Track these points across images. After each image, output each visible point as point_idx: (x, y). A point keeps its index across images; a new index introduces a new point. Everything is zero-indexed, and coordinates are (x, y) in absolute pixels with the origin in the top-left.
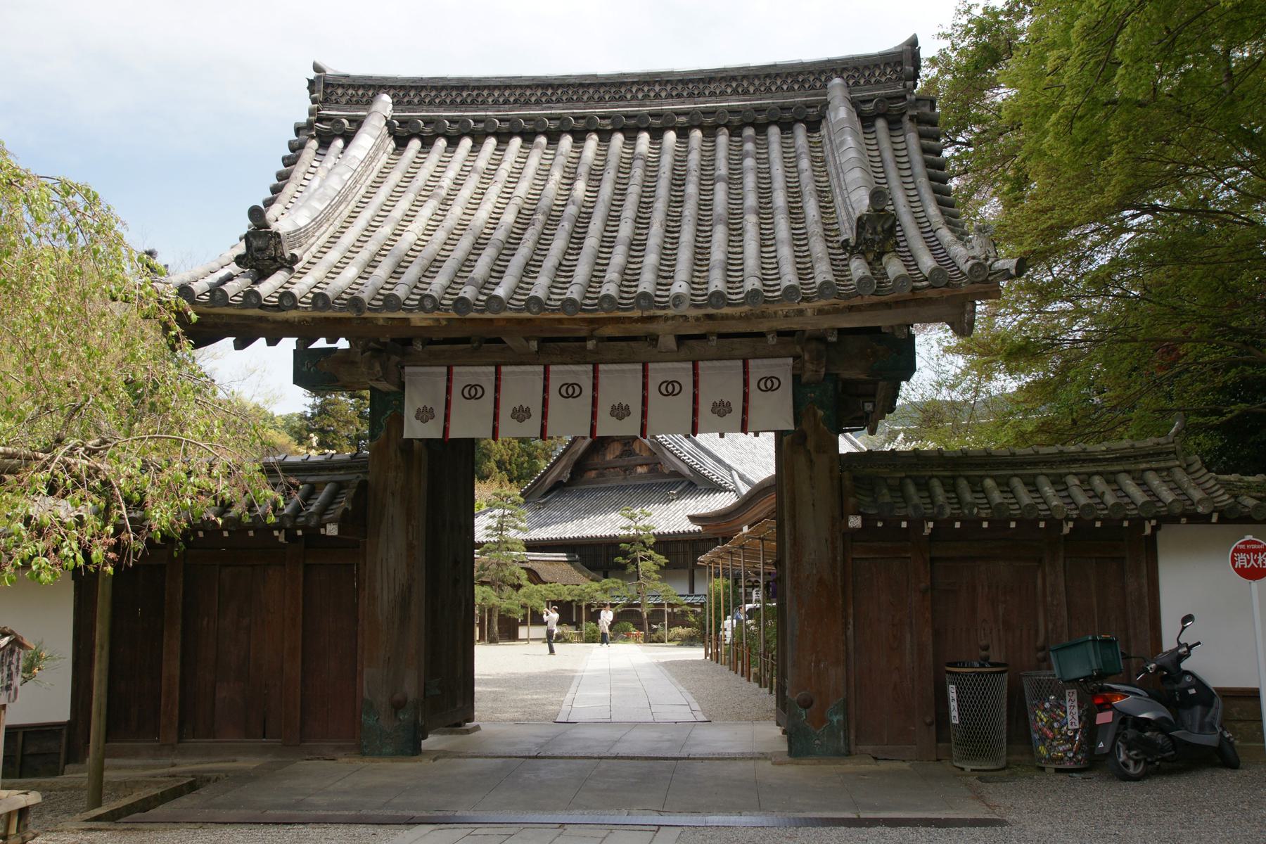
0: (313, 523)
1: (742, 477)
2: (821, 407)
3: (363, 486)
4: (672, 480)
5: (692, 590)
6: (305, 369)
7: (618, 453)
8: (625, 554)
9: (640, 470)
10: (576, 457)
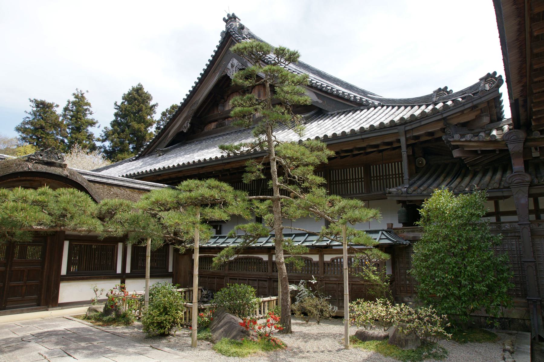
10: (195, 107)
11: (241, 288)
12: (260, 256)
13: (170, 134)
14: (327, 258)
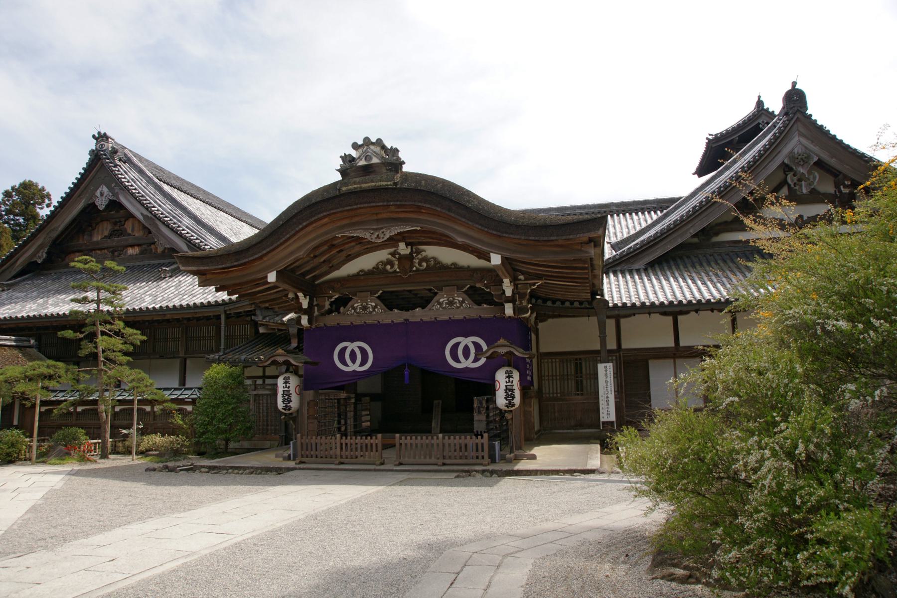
5: (183, 382)
7: (106, 233)
9: (130, 251)
10: (54, 235)
11: (74, 429)
12: (184, 407)
13: (19, 262)
14: (157, 408)
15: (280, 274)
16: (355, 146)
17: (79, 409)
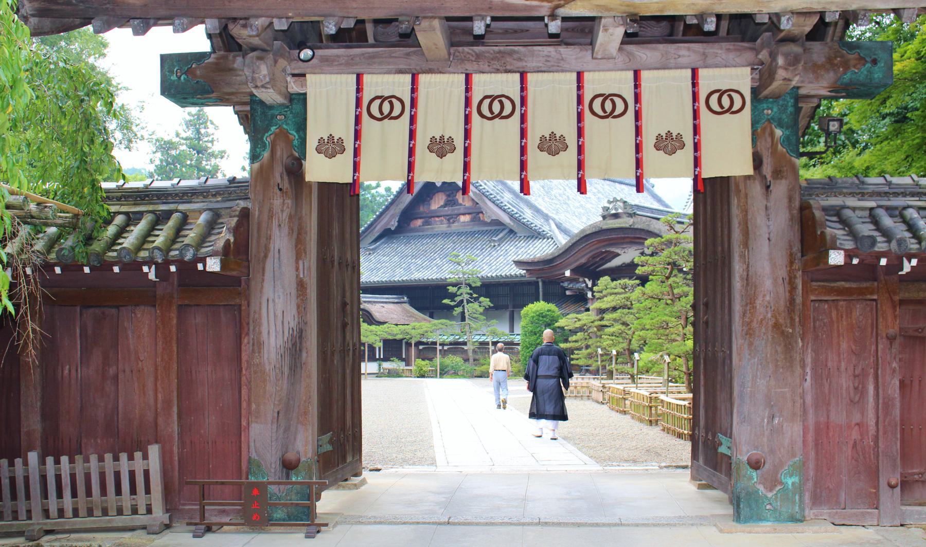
0: (189, 256)
1: (559, 226)
2: (780, 125)
3: (245, 215)
4: (494, 228)
6: (174, 78)
7: (442, 203)
8: (452, 296)
15: (572, 271)
16: (609, 202)
17: (446, 348)
